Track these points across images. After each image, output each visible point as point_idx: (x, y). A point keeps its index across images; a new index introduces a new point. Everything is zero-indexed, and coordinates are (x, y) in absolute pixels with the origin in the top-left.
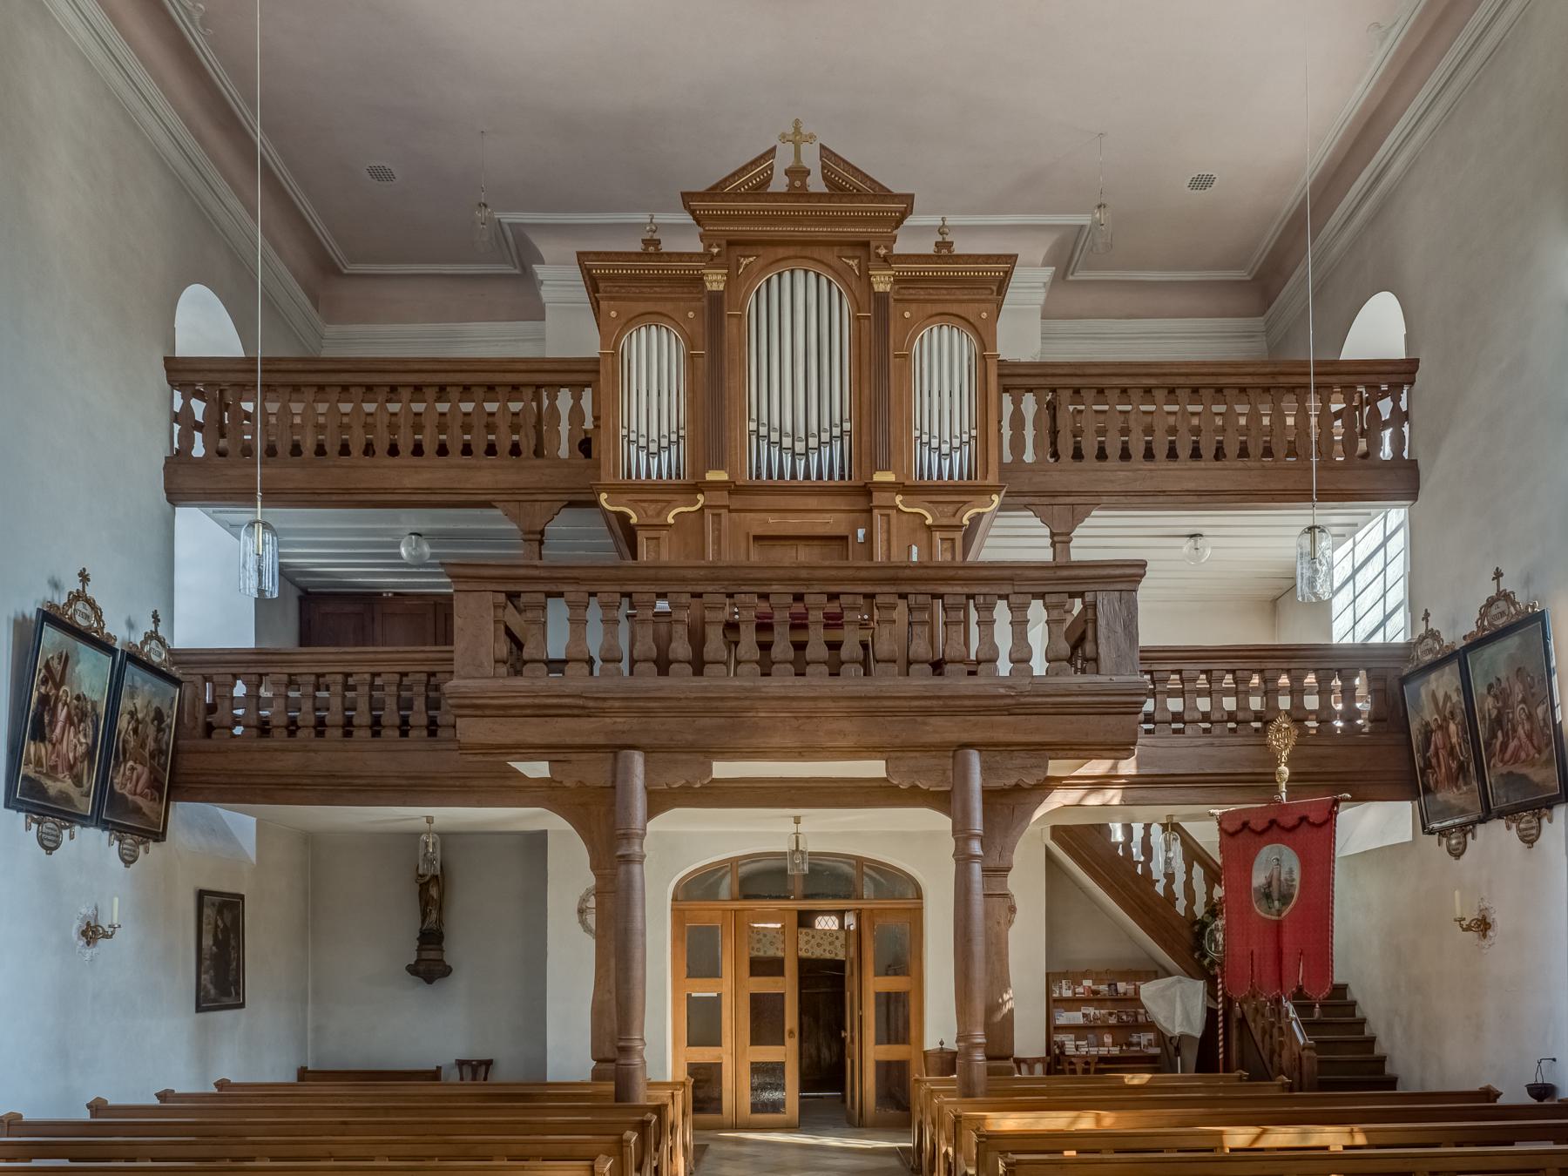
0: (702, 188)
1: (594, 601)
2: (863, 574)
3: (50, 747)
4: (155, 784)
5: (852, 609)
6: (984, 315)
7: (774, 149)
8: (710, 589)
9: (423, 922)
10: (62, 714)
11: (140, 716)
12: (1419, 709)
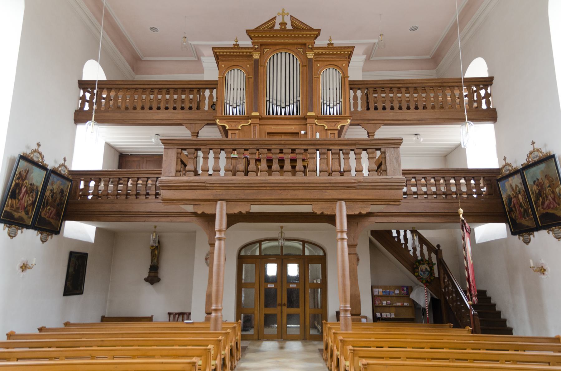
0: (253, 28)
1: (211, 152)
2: (303, 142)
3: (17, 201)
4: (58, 215)
5: (300, 154)
6: (344, 65)
7: (276, 17)
8: (251, 147)
9: (152, 263)
10: (24, 190)
11: (55, 191)
12: (505, 190)
